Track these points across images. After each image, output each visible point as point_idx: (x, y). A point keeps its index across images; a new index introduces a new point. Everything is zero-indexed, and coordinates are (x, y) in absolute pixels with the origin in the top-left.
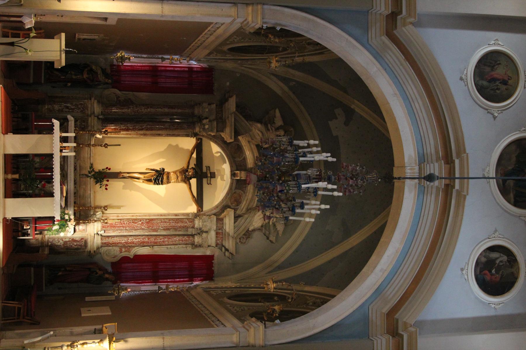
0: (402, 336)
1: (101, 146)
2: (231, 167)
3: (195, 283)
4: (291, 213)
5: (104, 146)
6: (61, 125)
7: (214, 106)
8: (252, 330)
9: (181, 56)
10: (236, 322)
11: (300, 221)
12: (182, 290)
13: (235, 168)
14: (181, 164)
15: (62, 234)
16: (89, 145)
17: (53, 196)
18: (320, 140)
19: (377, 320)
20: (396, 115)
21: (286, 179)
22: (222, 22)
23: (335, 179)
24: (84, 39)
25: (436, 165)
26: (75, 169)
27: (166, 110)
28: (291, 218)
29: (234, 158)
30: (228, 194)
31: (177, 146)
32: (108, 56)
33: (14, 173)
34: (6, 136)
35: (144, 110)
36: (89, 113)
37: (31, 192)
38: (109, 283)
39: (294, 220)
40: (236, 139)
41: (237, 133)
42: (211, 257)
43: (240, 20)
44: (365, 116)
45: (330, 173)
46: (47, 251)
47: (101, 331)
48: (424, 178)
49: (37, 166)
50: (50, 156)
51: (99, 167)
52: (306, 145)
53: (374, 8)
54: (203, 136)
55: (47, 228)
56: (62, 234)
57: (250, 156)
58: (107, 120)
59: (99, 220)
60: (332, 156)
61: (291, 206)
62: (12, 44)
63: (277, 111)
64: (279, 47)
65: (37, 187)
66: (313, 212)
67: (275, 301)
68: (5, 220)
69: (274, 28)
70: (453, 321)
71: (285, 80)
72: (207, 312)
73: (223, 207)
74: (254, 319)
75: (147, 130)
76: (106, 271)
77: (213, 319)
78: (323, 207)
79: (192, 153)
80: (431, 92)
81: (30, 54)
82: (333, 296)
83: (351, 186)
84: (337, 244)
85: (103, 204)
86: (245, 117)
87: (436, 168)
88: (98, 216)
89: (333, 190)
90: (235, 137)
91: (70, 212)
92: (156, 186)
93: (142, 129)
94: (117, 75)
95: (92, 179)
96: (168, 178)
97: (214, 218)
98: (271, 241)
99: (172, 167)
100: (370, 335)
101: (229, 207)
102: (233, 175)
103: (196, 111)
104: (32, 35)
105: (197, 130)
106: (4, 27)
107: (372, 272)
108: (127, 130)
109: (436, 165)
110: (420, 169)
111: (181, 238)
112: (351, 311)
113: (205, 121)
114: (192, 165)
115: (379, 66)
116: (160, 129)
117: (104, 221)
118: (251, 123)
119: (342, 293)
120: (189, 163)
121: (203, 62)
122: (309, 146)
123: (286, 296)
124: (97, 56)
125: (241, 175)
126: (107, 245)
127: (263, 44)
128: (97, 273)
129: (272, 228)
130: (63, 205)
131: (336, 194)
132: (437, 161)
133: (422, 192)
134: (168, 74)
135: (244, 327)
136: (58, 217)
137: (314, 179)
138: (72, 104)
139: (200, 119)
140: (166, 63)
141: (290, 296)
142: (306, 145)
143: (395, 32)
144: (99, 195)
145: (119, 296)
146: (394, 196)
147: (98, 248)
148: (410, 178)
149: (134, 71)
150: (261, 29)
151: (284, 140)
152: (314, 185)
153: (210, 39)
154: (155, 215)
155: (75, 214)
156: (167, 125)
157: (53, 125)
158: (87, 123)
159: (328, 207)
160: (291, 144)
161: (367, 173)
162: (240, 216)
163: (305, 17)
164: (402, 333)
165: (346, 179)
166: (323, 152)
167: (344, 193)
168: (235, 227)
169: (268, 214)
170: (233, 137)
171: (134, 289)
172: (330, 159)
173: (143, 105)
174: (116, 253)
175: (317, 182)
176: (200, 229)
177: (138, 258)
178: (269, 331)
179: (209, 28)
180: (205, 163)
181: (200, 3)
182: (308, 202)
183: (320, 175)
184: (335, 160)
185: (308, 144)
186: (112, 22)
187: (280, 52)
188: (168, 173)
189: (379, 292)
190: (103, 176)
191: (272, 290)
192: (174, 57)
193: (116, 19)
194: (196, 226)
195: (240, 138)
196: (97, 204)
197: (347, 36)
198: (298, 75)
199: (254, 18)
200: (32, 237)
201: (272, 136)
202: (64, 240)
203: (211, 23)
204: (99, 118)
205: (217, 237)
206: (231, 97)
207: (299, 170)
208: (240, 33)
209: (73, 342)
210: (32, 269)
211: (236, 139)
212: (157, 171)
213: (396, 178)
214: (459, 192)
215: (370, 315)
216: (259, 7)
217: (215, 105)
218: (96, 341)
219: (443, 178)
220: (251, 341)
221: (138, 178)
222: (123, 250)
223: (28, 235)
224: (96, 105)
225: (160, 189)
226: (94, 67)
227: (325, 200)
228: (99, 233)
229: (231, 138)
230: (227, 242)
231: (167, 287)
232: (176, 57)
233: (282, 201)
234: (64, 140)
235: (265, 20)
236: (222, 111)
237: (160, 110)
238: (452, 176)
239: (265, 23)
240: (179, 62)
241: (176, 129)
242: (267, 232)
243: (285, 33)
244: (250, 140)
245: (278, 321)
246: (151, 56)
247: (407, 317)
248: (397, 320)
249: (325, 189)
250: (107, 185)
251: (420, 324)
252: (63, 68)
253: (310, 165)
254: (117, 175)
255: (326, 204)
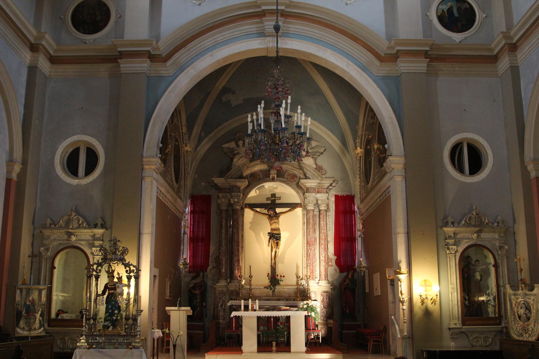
0: (398, 51)
1: (251, 281)
2: (267, 181)
3: (356, 209)
4: (303, 136)
5: (251, 278)
6: (235, 310)
7: (220, 195)
8: (393, 166)
9: (182, 219)
10: (386, 178)
11: (310, 129)
12: (362, 219)
13: (267, 179)
14: (265, 220)
15: (318, 310)
16: (250, 289)
17: (289, 316)
18: (247, 112)
19: (386, 69)
20: (237, 51)
21: (277, 139)
22: (156, 188)
23: (278, 101)
24: (170, 293)
25: (266, 23)
26: (269, 300)
27: (223, 231)
28: (308, 136)
29: (260, 179)
30: (288, 184)
31: (250, 223)
32: (182, 275)
33: (272, 346)
34: (243, 351)
35: (224, 248)
36: (226, 289)
37: (286, 333)
38: (356, 274)
39: (309, 133)
40: (246, 178)
41: (241, 177)
42: (337, 197)
43: (155, 175)
44: (227, 80)
45: (273, 106)
46: (331, 321)
47: (392, 281)
48: (277, 33)
49: (266, 329)
50: (259, 318)
51: (266, 281)
52: (251, 124)
53: (145, 71)
54: (243, 203)
55: (314, 321)
56: (318, 310)
57: (259, 167)
58: (231, 276)
59: (307, 282)
60: (260, 104)
61: (299, 136)
62: (175, 346)
63: (224, 146)
64: (175, 144)
65: (282, 328)
66: (303, 118)
67: (370, 148)
68: (307, 352)
69: (161, 149)
70: (386, 12)
71: (200, 140)
72: (378, 200)
73: (299, 187)
74: (385, 165)
75: (239, 246)
76: (346, 277)
77: (384, 195)
78: (299, 111)
79: (257, 211)
80: (200, 32)
81: (181, 333)
82: (367, 103)
83: (283, 89)
84: (327, 100)
85: (295, 279)
86: (228, 171)
87: (269, 24)
88: (305, 283)
89: (287, 103)
90: (244, 178)
91: (301, 304)
92: (282, 239)
93: (238, 250)
94: (197, 268)
95: (276, 287)
96: (275, 230)
97: (306, 194)
98: (324, 151)
99: (267, 227)
100: (397, 75)
101: (298, 183)
102: (273, 180)
103: (224, 208)
104: (167, 331)
105: (238, 207)
106: (162, 352)
107: (348, 73)
108: (238, 261)
109: (266, 23)
110: (269, 36)
111: (321, 220)
112: (378, 89)
113: (232, 202)
114: (266, 211)
115: (190, 68)
116: (238, 236)
117: (308, 278)
118: (233, 166)
119: (365, 96)
120: (264, 214)
121: (186, 203)
122: (252, 121)
123: (367, 140)
124: (183, 283)
125: (273, 173)
126: (326, 276)
127: (172, 157)
128: (348, 284)
129: (314, 150)
130: (297, 309)
131: (289, 101)
132: (263, 23)
133: (287, 35)
134: (196, 229)
135: (390, 172)
136: (306, 313)
137: (278, 118)
138: (219, 302)
139: (230, 205)
140: (188, 231)
141: (367, 136)
142: (251, 124)
143: (163, 56)
144: (289, 282)
145: (365, 267)
146: (290, 56)
147: (329, 283)
148: (277, 44)
149: (193, 256)
150: (161, 158)
151: (247, 140)
152: (283, 118)
153: (169, 197)
154: (304, 240)
155: (303, 300)
156: (235, 231)
157: (235, 317)
158: (234, 291)
159: (299, 107)
160: (251, 135)
161: (273, 77)
162: (305, 175)
163: (153, 124)
164: (395, 51)
165: (278, 93)
166: (257, 110)
167: (289, 94)
168: (314, 179)
169: (304, 153)
170: (244, 180)
171: (360, 256)
172: (263, 105)
173: (220, 249)
174: (333, 269)
175: (280, 116)
176: (315, 205)
177: (337, 252)
178: (394, 153)
179: (161, 198)
180: (264, 201)
181: (142, 205)
182: (295, 123)
183: (275, 113)
184: (263, 102)
185: (251, 122)
186: (157, 272)
187: (178, 144)
188: (272, 229)
189: (364, 69)
190: (274, 279)
191: (362, 150)
192: (183, 225)
193: (155, 269)
194: (312, 208)
195: (245, 175)
196: (295, 283)
197: (167, 93)
198: (197, 129)
199: (152, 164)
200: (321, 332)
201: (243, 150)
202: (322, 308)
203: (158, 198)
204: (230, 282)
205: (321, 193)
206: (213, 181)
207: (270, 129)
208: (164, 175)
209: (400, 301)
210: (344, 332)
211: (246, 178)
212: (270, 238)
213: (277, 55)
214: (287, 6)
215: (382, 75)
216: (144, 160)
217: (220, 194)
218: (399, 284)
219: (277, 19)
220: (401, 166)
221: (276, 252)
222: (330, 264)
223: (318, 335)
224: (219, 284)
225: (284, 236)
226: (191, 286)
227: (294, 109)
228: (317, 282)
229: (245, 181)
230: (325, 185)
231: (359, 231)
232: (183, 223)
233: (295, 142)
234: (246, 308)
235: (155, 156)
236: (224, 189)
237: (223, 236)
238: (276, 12)
239: (157, 155)
240: (187, 221)
241: (238, 224)
242: (318, 154)
243: (164, 140)
244: (246, 167)
245: (386, 146)
246: (182, 244)
247: (383, 47)
248: (386, 54)
249: (286, 109)
250: (281, 276)
251: (389, 37)
252: (192, 309)
253: (266, 121)
254: (273, 268)
255: (297, 109)
